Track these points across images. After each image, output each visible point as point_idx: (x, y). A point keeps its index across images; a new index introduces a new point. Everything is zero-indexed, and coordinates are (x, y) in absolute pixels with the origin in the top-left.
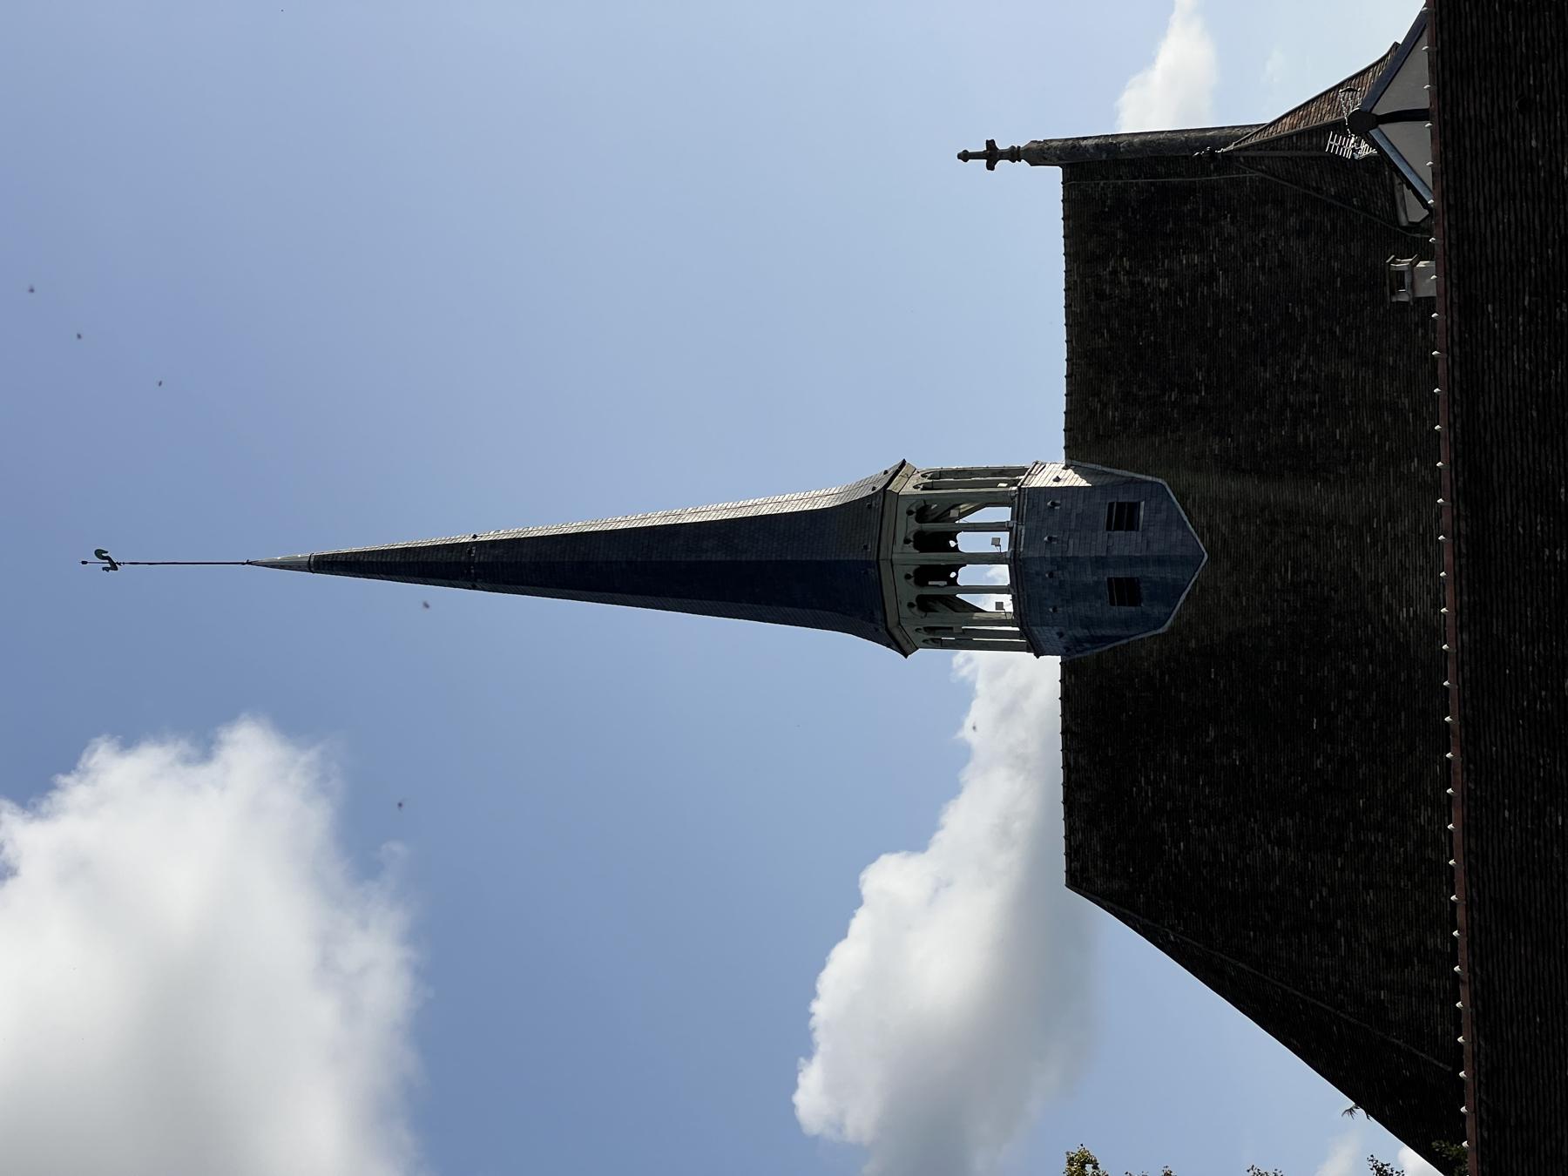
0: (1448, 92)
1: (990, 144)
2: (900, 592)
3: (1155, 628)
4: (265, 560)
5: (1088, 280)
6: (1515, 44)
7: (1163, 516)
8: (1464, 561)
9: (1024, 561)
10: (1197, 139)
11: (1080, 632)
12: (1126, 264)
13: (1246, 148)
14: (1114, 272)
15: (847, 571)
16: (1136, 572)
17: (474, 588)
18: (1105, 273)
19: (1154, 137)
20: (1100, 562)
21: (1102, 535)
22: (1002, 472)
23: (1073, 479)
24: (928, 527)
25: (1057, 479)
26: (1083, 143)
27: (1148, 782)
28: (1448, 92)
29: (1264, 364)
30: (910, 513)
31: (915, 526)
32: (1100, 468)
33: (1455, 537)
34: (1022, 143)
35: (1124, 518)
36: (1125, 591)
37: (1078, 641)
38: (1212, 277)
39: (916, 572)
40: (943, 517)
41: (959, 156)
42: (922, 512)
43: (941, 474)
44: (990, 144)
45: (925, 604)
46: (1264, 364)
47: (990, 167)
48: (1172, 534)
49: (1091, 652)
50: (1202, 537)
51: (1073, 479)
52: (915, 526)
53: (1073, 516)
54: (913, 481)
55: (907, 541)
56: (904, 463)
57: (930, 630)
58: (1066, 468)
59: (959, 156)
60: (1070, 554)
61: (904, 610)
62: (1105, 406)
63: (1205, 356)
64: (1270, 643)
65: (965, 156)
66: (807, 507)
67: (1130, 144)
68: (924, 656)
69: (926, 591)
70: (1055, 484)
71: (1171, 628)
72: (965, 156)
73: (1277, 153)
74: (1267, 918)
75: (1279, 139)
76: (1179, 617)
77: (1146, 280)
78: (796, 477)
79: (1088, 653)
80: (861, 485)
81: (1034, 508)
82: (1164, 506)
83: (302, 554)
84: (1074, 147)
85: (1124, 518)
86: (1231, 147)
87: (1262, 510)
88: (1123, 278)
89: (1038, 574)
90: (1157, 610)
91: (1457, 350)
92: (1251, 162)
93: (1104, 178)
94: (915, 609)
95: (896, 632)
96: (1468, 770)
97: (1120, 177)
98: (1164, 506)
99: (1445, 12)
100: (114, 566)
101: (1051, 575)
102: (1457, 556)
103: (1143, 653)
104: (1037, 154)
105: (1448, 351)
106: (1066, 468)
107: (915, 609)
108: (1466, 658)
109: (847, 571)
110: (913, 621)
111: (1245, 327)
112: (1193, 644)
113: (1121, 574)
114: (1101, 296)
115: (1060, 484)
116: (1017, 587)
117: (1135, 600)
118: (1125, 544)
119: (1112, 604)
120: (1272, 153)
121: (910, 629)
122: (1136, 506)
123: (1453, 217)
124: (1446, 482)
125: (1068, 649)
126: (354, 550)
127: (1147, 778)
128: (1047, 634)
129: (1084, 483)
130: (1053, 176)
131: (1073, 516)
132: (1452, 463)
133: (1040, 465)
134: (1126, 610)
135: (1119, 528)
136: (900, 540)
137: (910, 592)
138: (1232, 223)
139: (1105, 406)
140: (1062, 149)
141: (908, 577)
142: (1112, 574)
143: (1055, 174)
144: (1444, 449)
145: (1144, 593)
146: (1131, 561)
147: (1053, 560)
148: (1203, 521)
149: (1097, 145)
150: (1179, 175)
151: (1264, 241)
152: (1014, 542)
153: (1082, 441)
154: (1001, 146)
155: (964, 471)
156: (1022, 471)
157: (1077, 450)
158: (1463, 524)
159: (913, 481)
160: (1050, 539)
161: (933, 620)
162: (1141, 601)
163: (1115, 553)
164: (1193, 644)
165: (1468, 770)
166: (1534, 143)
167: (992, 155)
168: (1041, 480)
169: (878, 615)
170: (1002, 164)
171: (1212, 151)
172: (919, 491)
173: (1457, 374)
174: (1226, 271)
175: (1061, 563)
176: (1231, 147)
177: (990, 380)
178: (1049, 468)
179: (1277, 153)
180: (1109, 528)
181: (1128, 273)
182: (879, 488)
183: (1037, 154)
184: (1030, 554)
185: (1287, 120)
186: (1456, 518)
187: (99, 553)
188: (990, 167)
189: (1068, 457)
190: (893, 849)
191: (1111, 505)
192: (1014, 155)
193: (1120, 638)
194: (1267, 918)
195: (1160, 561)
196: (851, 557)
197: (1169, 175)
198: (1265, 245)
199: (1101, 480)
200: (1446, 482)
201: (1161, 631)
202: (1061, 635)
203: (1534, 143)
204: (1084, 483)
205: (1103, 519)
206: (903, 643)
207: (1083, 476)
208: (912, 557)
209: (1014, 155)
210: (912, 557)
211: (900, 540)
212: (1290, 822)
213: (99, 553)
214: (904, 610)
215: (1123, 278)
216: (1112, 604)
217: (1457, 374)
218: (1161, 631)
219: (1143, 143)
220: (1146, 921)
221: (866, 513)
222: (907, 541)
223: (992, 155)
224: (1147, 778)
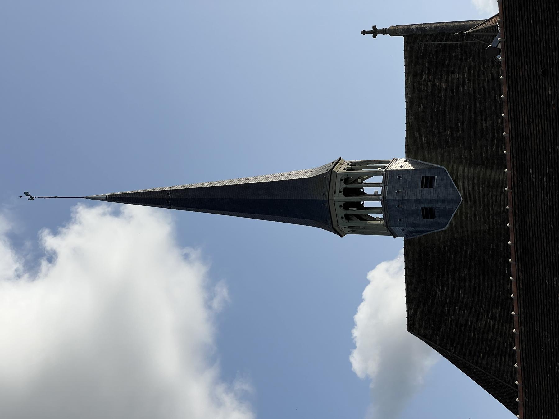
0: (510, 62)
1: (374, 27)
2: (338, 213)
3: (442, 228)
4: (89, 196)
5: (415, 84)
6: (540, 41)
7: (444, 182)
8: (521, 292)
9: (388, 201)
10: (457, 26)
11: (411, 229)
12: (430, 77)
13: (476, 31)
14: (425, 81)
15: (317, 202)
16: (434, 206)
17: (170, 208)
18: (421, 81)
19: (441, 25)
20: (418, 201)
21: (419, 189)
22: (380, 162)
23: (408, 166)
24: (349, 186)
25: (402, 166)
26: (412, 27)
27: (439, 291)
28: (510, 62)
29: (486, 121)
30: (342, 180)
31: (344, 186)
32: (419, 161)
33: (518, 279)
34: (387, 27)
35: (428, 183)
36: (429, 213)
37: (411, 232)
38: (464, 84)
39: (344, 204)
40: (355, 181)
41: (362, 33)
42: (347, 180)
43: (354, 164)
44: (374, 27)
45: (348, 217)
46: (485, 120)
47: (374, 37)
48: (448, 190)
49: (416, 237)
50: (460, 191)
51: (408, 166)
52: (344, 186)
53: (408, 182)
54: (344, 167)
55: (340, 192)
56: (340, 158)
57: (350, 227)
58: (406, 161)
59: (362, 33)
60: (406, 198)
61: (340, 220)
62: (421, 136)
63: (461, 116)
64: (488, 237)
65: (364, 33)
66: (301, 177)
67: (431, 28)
68: (350, 237)
69: (348, 212)
70: (400, 169)
71: (448, 228)
72: (364, 33)
73: (489, 34)
74: (488, 349)
75: (490, 28)
76: (451, 223)
77: (438, 84)
78: (297, 164)
79: (415, 237)
80: (323, 167)
81: (391, 177)
82: (445, 178)
83: (104, 194)
84: (408, 28)
85: (428, 183)
86: (470, 31)
87: (485, 181)
88: (429, 83)
89: (393, 206)
90: (442, 221)
91: (516, 189)
92: (478, 37)
93: (420, 41)
94: (344, 219)
95: (337, 228)
96: (525, 392)
97: (427, 41)
98: (445, 178)
99: (507, 22)
100: (32, 198)
101: (398, 206)
102: (518, 288)
103: (437, 238)
104: (393, 31)
105: (512, 188)
106: (406, 161)
107: (344, 219)
108: (523, 338)
109: (317, 202)
110: (343, 224)
111: (478, 104)
112: (457, 235)
113: (427, 206)
114: (419, 90)
115: (402, 169)
116: (385, 209)
117: (433, 217)
118: (429, 194)
119: (424, 218)
120: (486, 34)
121: (342, 227)
122: (432, 178)
123: (513, 124)
124: (512, 252)
125: (407, 235)
126: (124, 192)
127: (439, 289)
128: (399, 229)
129: (411, 168)
130: (400, 40)
131: (408, 182)
132: (515, 243)
133: (395, 160)
134: (430, 220)
135: (426, 187)
136: (337, 192)
137: (342, 212)
138: (473, 61)
139: (421, 136)
140: (403, 30)
141: (341, 206)
142: (423, 206)
143: (401, 39)
144: (512, 236)
145: (436, 214)
146: (431, 201)
147: (399, 200)
148: (461, 185)
149: (417, 28)
150: (451, 40)
151: (485, 69)
152: (384, 191)
153: (413, 150)
154: (379, 28)
155: (365, 162)
156: (388, 162)
157: (410, 155)
158: (520, 274)
159: (344, 167)
160: (398, 191)
161: (351, 224)
162: (435, 217)
163: (424, 198)
164: (457, 235)
165: (525, 392)
166: (550, 92)
167: (375, 32)
168: (395, 167)
169: (329, 221)
170: (379, 36)
171: (462, 33)
172: (345, 171)
173: (516, 201)
174: (470, 81)
175: (403, 201)
176: (470, 31)
177: (373, 127)
178: (399, 161)
179: (489, 34)
180: (422, 187)
181: (430, 81)
182: (329, 169)
183: (393, 31)
184: (390, 198)
185: (493, 19)
186: (518, 270)
187: (26, 193)
188: (374, 37)
189: (407, 156)
190: (384, 261)
191: (423, 177)
192: (384, 32)
193: (427, 231)
194: (488, 349)
195: (443, 201)
196: (318, 198)
197: (447, 40)
198: (486, 70)
199: (421, 167)
200: (512, 252)
201: (444, 229)
202: (403, 230)
203: (550, 92)
204: (411, 168)
205: (420, 184)
206: (340, 232)
207: (412, 165)
208: (343, 198)
209: (384, 32)
210: (343, 198)
211: (337, 192)
212: (497, 311)
213: (26, 193)
214: (340, 220)
215: (429, 83)
216: (424, 218)
217: (516, 201)
218: (444, 229)
219: (436, 27)
220: (439, 347)
221: (325, 179)
222: (340, 192)
223: (375, 32)
224: (439, 289)
